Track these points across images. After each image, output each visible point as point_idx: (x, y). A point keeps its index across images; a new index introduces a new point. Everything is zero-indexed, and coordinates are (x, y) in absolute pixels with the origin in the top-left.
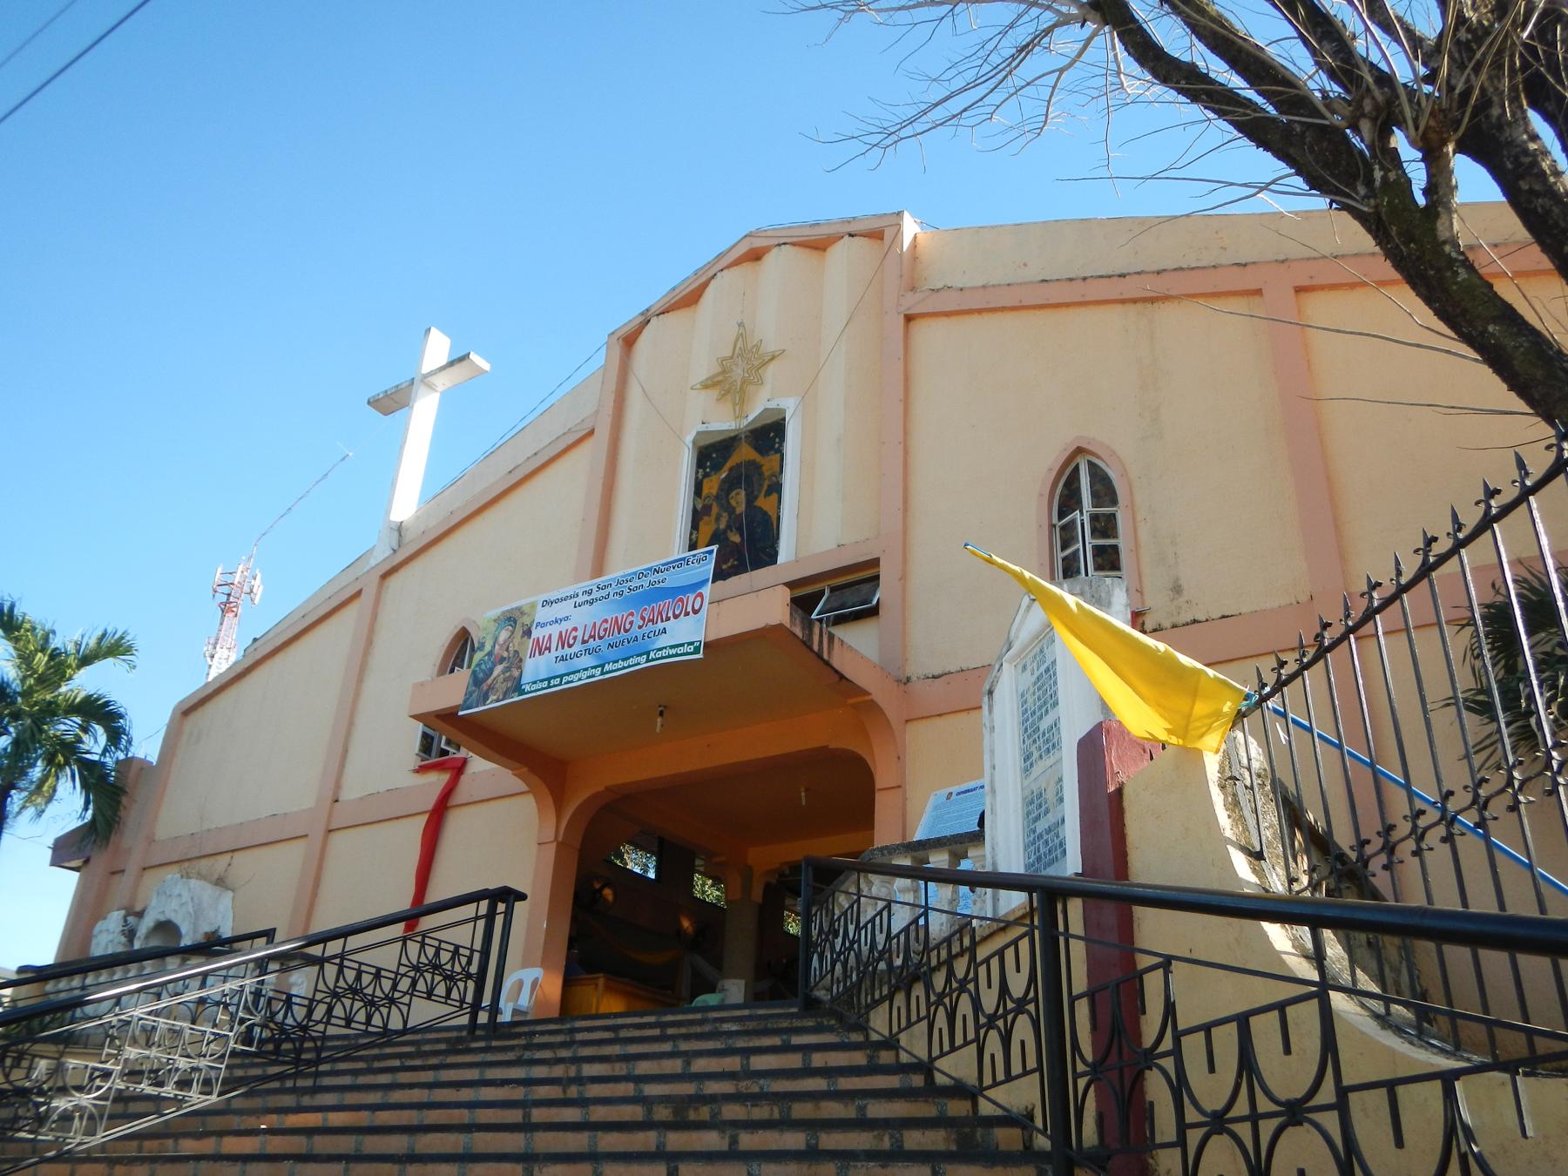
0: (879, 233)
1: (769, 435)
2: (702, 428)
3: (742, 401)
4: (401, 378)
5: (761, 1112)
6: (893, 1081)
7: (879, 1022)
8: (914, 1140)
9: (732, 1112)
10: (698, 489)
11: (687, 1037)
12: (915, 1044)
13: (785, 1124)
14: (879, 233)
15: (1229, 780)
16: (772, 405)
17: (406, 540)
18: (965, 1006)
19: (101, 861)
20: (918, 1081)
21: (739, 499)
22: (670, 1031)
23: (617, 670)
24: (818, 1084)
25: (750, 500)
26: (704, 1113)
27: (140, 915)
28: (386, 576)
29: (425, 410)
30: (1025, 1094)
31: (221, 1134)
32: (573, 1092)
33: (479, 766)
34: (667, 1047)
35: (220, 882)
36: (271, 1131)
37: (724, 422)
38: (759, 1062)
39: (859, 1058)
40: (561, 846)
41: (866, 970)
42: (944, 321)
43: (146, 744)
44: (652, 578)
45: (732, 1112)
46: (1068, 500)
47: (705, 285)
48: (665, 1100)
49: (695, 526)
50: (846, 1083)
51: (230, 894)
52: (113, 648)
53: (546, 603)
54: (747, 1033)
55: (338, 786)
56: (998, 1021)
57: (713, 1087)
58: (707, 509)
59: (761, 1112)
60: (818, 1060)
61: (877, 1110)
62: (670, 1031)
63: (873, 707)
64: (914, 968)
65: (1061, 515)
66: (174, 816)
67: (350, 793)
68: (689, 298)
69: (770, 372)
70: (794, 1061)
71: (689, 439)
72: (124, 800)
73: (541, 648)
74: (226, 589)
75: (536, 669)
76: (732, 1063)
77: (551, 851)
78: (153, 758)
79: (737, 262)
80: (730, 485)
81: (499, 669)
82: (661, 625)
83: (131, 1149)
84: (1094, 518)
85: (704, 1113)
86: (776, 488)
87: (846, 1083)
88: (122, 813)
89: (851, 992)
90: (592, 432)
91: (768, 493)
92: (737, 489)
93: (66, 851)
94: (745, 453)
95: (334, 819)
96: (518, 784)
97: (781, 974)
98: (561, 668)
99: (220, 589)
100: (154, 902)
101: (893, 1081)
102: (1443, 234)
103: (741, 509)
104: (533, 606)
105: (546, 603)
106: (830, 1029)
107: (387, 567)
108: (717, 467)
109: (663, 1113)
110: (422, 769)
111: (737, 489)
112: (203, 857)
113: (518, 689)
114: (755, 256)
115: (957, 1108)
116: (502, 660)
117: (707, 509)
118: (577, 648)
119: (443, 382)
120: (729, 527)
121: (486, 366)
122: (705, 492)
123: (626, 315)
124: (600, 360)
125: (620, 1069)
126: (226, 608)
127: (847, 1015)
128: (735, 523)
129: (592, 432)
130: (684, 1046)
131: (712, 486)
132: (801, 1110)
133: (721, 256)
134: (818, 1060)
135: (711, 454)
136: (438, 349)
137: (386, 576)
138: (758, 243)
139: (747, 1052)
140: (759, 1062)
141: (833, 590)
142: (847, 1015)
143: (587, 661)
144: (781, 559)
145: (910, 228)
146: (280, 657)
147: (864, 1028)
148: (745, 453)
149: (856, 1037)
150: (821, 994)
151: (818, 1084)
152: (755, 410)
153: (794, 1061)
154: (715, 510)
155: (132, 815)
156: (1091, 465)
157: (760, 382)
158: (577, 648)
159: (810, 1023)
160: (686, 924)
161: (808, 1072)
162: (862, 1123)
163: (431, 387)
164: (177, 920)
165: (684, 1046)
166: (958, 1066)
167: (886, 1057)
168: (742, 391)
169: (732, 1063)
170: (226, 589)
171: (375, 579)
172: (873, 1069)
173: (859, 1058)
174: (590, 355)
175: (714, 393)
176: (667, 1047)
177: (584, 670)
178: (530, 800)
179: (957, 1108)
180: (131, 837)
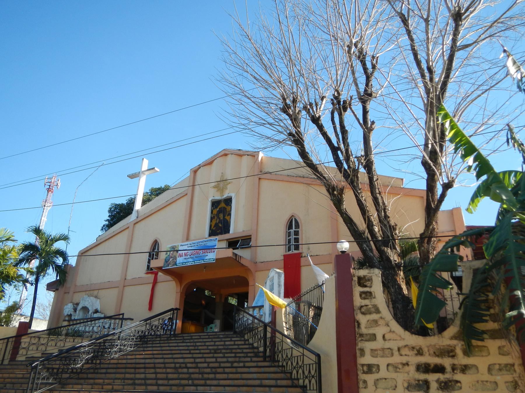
0: (254, 155)
1: (228, 201)
2: (213, 198)
3: (222, 192)
4: (136, 171)
5: (228, 351)
6: (247, 346)
7: (246, 337)
8: (249, 355)
9: (224, 351)
10: (212, 212)
11: (214, 338)
12: (251, 341)
13: (232, 353)
14: (254, 155)
15: (285, 313)
16: (229, 195)
17: (140, 215)
18: (256, 337)
19: (62, 290)
20: (251, 346)
21: (221, 216)
22: (210, 337)
23: (197, 263)
24: (236, 347)
25: (224, 217)
26: (219, 351)
27: (77, 304)
28: (135, 224)
29: (143, 180)
30: (261, 349)
31: (136, 355)
32: (196, 348)
33: (160, 274)
34: (210, 340)
35: (96, 297)
36: (145, 354)
37: (218, 197)
38: (227, 343)
39: (243, 343)
40: (181, 293)
41: (245, 329)
42: (267, 181)
43: (73, 261)
44: (205, 243)
45: (224, 351)
46: (290, 227)
47: (214, 160)
48: (213, 349)
49: (211, 221)
50: (241, 347)
51: (99, 300)
52: (65, 238)
53: (181, 245)
54: (224, 338)
55: (126, 275)
56: (260, 340)
57: (220, 347)
58: (214, 217)
59: (228, 351)
60: (236, 343)
61: (245, 351)
62: (210, 337)
63: (249, 270)
64: (250, 329)
65: (289, 230)
66: (82, 279)
67: (129, 277)
68: (210, 163)
69: (229, 186)
70: (232, 343)
71: (210, 200)
72: (67, 275)
73: (181, 256)
74: (49, 184)
75: (180, 260)
76: (222, 343)
77: (179, 295)
78: (74, 265)
79: (222, 156)
80: (219, 212)
81: (171, 259)
82: (206, 254)
83: (122, 357)
84: (295, 231)
85: (219, 351)
86: (230, 215)
87: (241, 347)
88: (67, 278)
89: (242, 331)
90: (187, 194)
91: (228, 215)
92: (221, 211)
93: (50, 287)
94: (223, 205)
95: (125, 283)
96: (172, 279)
97: (228, 326)
98: (185, 261)
99: (47, 184)
100: (81, 302)
101: (247, 346)
102: (342, 208)
103: (222, 218)
104: (178, 246)
105: (181, 245)
106: (238, 337)
107: (135, 222)
108: (216, 207)
109: (213, 351)
110: (147, 273)
111: (221, 211)
112: (92, 290)
113: (176, 264)
114: (226, 155)
115: (256, 350)
116: (172, 257)
117: (214, 217)
118: (188, 257)
119: (147, 173)
120: (219, 222)
121: (158, 170)
122: (214, 213)
123: (195, 165)
124: (189, 174)
125: (203, 344)
126: (49, 190)
127: (241, 334)
128: (220, 222)
129: (187, 194)
130: (214, 340)
131: (215, 212)
132: (234, 351)
133: (217, 154)
134: (236, 343)
135: (215, 204)
136: (145, 166)
137: (135, 224)
138: (227, 152)
139: (225, 341)
140: (227, 343)
141: (242, 240)
142: (241, 334)
143: (191, 260)
144: (231, 232)
145: (261, 155)
146: (107, 242)
147: (244, 337)
148: (223, 205)
149: (243, 339)
150: (237, 330)
151: (236, 347)
152: (225, 196)
153: (232, 343)
154: (216, 218)
155: (69, 278)
156: (295, 219)
157: (226, 189)
158: (188, 257)
159: (235, 336)
160: (203, 302)
161: (235, 345)
162: (242, 353)
163: (144, 174)
164: (88, 306)
165: (214, 340)
166: (255, 345)
167: (247, 342)
168: (222, 190)
169: (222, 343)
170: (49, 184)
171: (133, 225)
172: (245, 344)
173: (243, 343)
174: (186, 174)
175: (216, 189)
176: (210, 340)
177: (190, 262)
178: (174, 282)
179: (256, 350)
180: (68, 284)
